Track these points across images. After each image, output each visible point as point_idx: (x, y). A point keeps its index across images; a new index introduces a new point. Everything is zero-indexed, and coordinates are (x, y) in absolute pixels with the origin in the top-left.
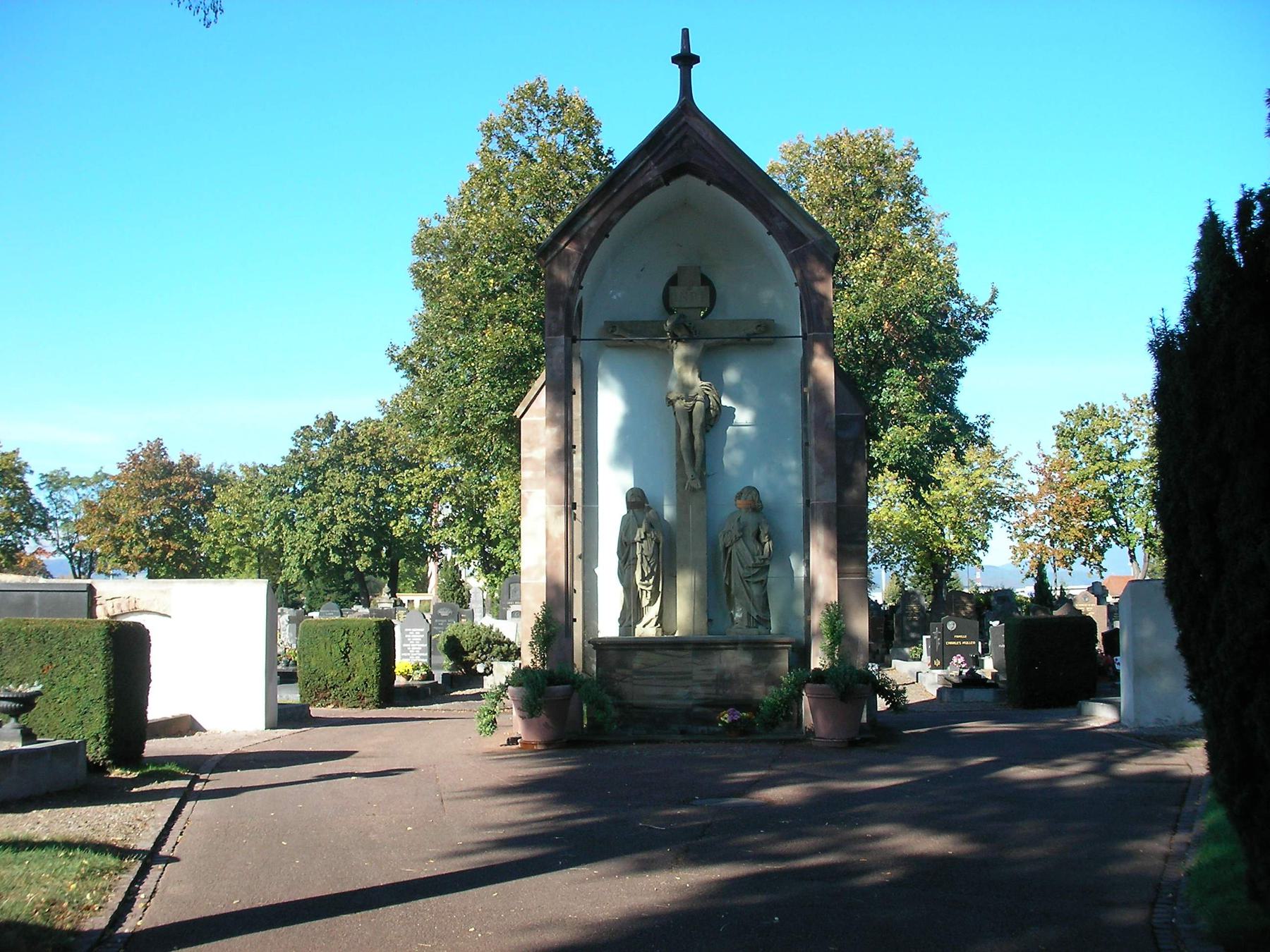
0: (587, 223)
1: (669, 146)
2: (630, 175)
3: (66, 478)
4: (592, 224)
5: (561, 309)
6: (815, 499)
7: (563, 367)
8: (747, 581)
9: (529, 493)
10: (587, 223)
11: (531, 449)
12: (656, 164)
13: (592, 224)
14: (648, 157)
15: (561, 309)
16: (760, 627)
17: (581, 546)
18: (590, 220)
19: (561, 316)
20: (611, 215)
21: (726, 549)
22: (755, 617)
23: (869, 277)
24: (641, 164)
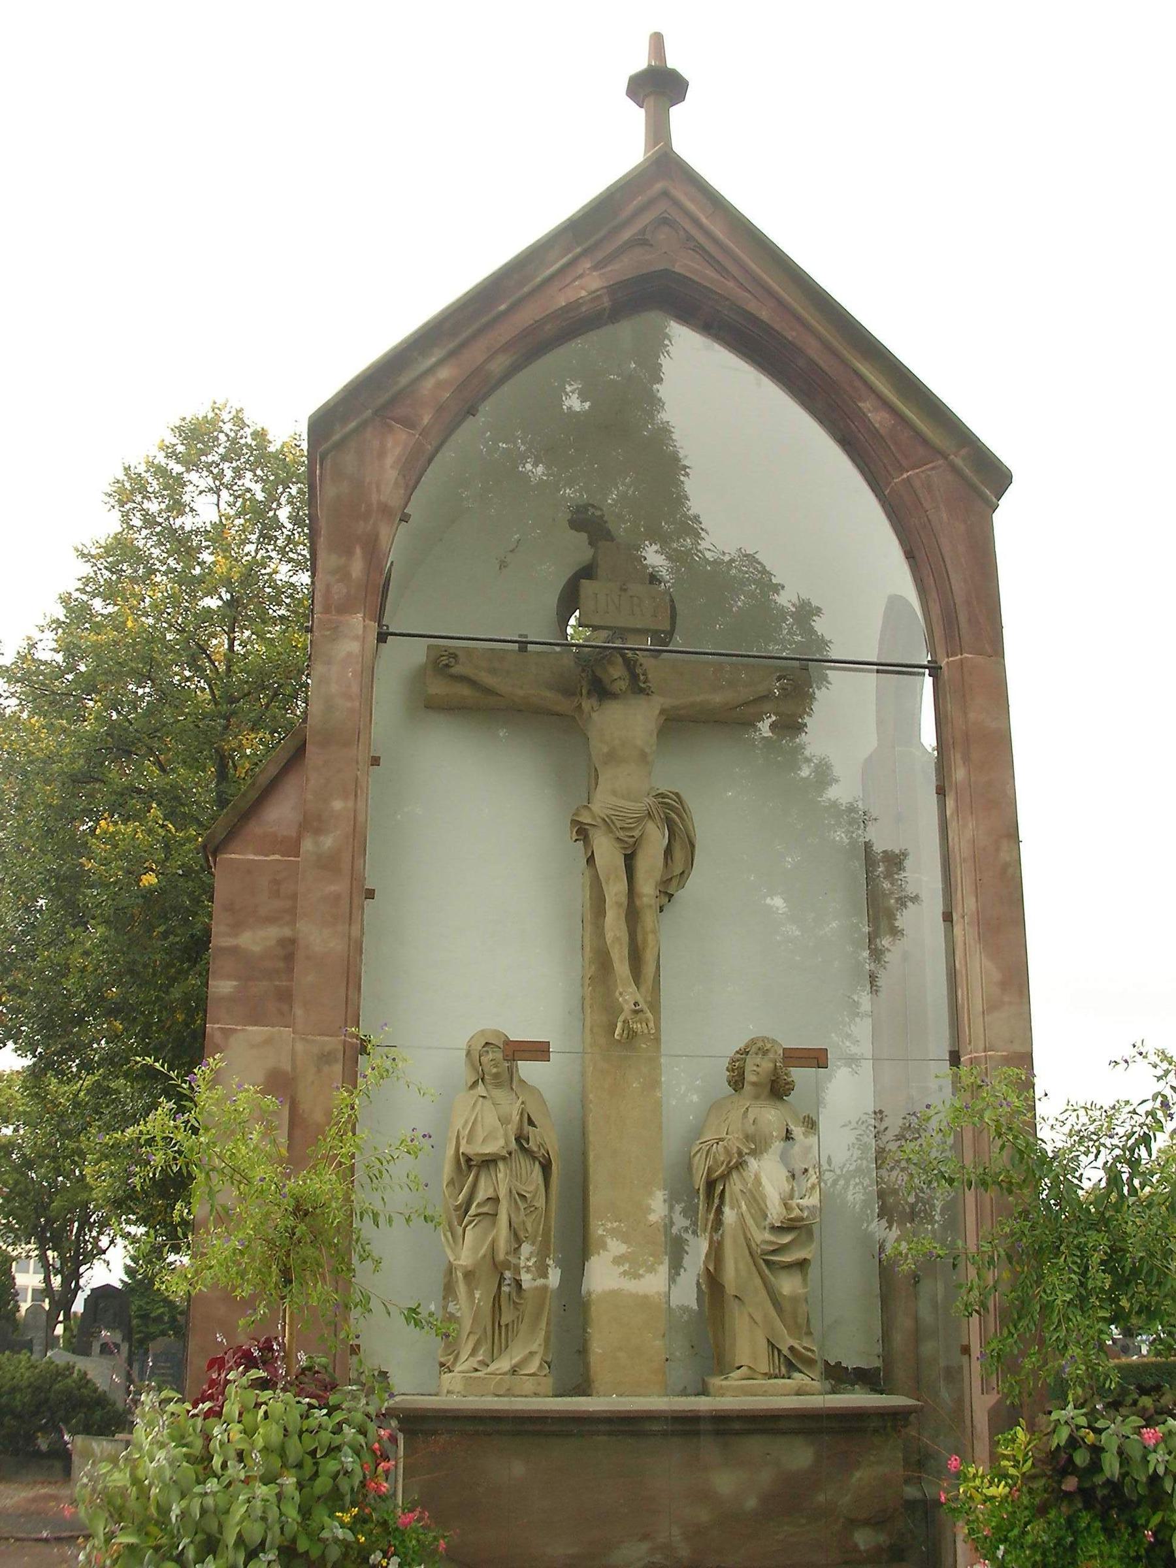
0: (431, 370)
1: (626, 235)
2: (539, 279)
3: (57, 1371)
4: (444, 374)
5: (358, 551)
6: (981, 1046)
7: (355, 689)
8: (767, 1262)
9: (227, 1033)
10: (431, 370)
11: (237, 927)
12: (595, 268)
13: (444, 374)
14: (578, 250)
15: (358, 551)
16: (796, 1375)
17: (945, 992)
18: (441, 363)
19: (357, 567)
20: (490, 358)
21: (711, 1185)
22: (785, 1351)
23: (104, 1181)
24: (565, 260)
